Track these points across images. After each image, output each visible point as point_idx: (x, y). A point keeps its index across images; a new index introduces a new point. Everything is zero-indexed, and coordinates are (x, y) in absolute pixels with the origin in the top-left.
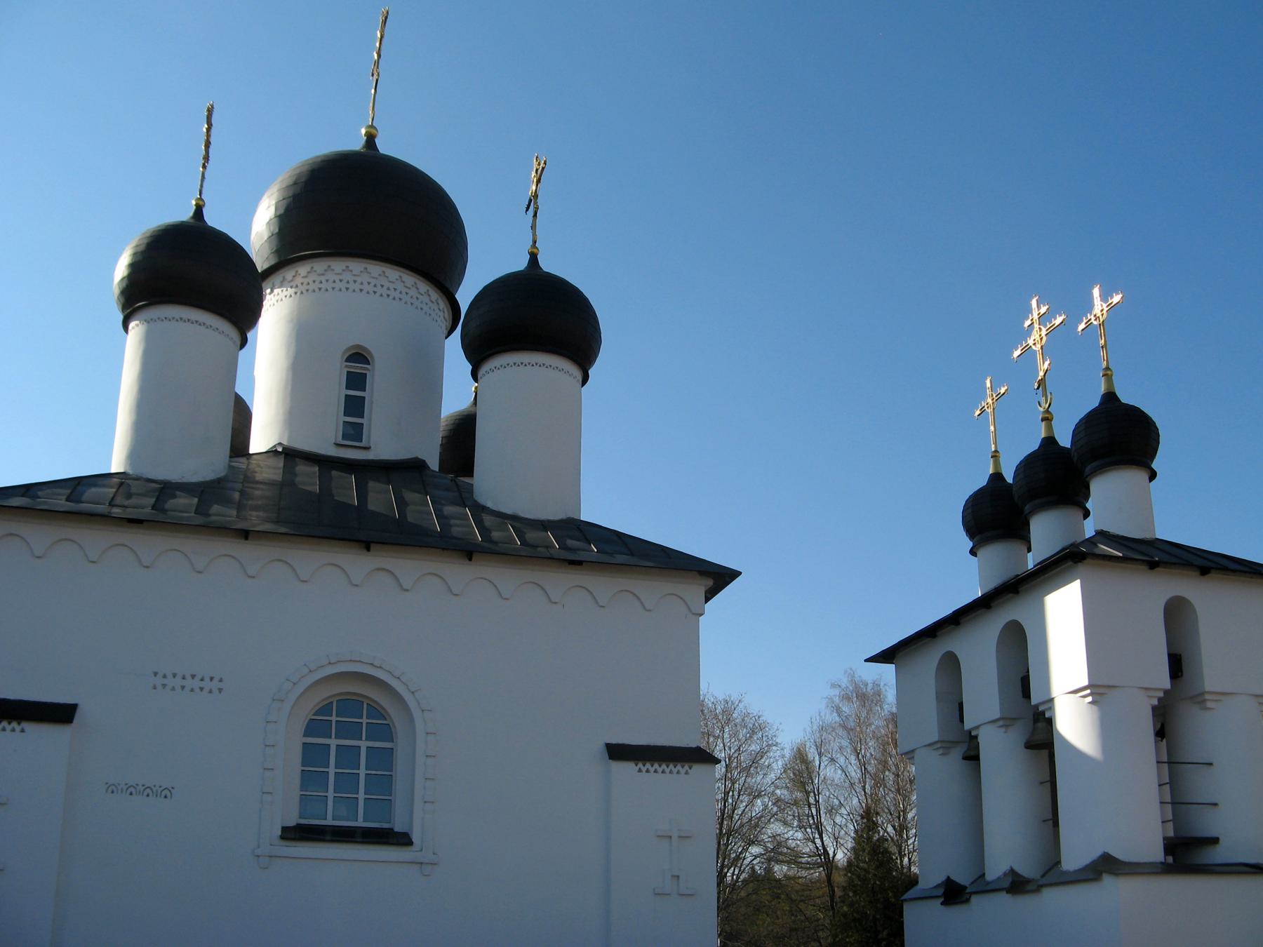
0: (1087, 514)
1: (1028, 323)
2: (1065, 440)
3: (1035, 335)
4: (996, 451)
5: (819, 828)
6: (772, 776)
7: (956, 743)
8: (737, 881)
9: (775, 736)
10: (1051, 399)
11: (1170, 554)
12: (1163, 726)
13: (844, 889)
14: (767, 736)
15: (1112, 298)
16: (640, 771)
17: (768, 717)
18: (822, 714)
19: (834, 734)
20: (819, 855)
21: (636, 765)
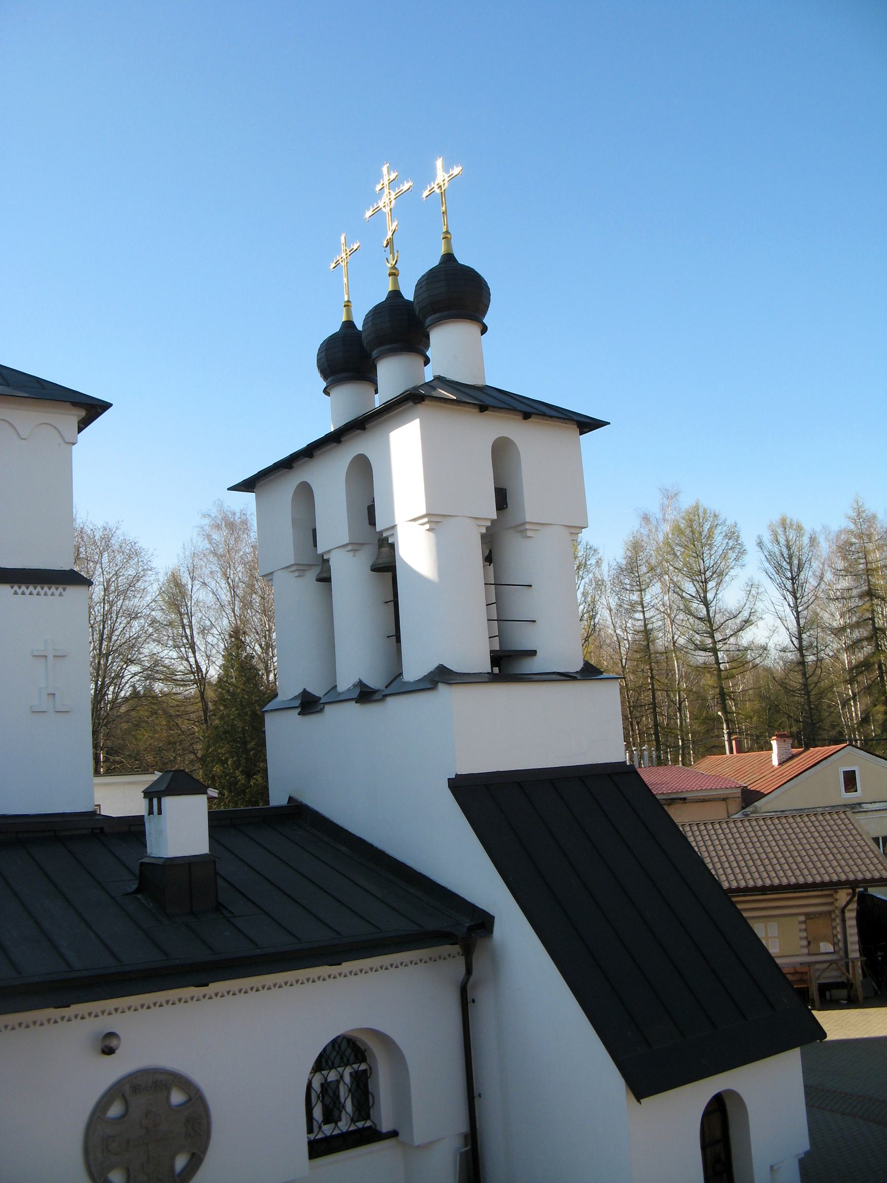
0: (427, 361)
1: (379, 187)
2: (409, 294)
3: (385, 199)
4: (349, 301)
5: (193, 646)
6: (149, 599)
7: (310, 566)
8: (116, 699)
9: (150, 561)
10: (397, 257)
11: (495, 398)
12: (490, 552)
13: (215, 703)
14: (143, 561)
15: (453, 169)
16: (16, 593)
17: (143, 543)
18: (194, 541)
19: (205, 560)
20: (193, 673)
21: (12, 588)
